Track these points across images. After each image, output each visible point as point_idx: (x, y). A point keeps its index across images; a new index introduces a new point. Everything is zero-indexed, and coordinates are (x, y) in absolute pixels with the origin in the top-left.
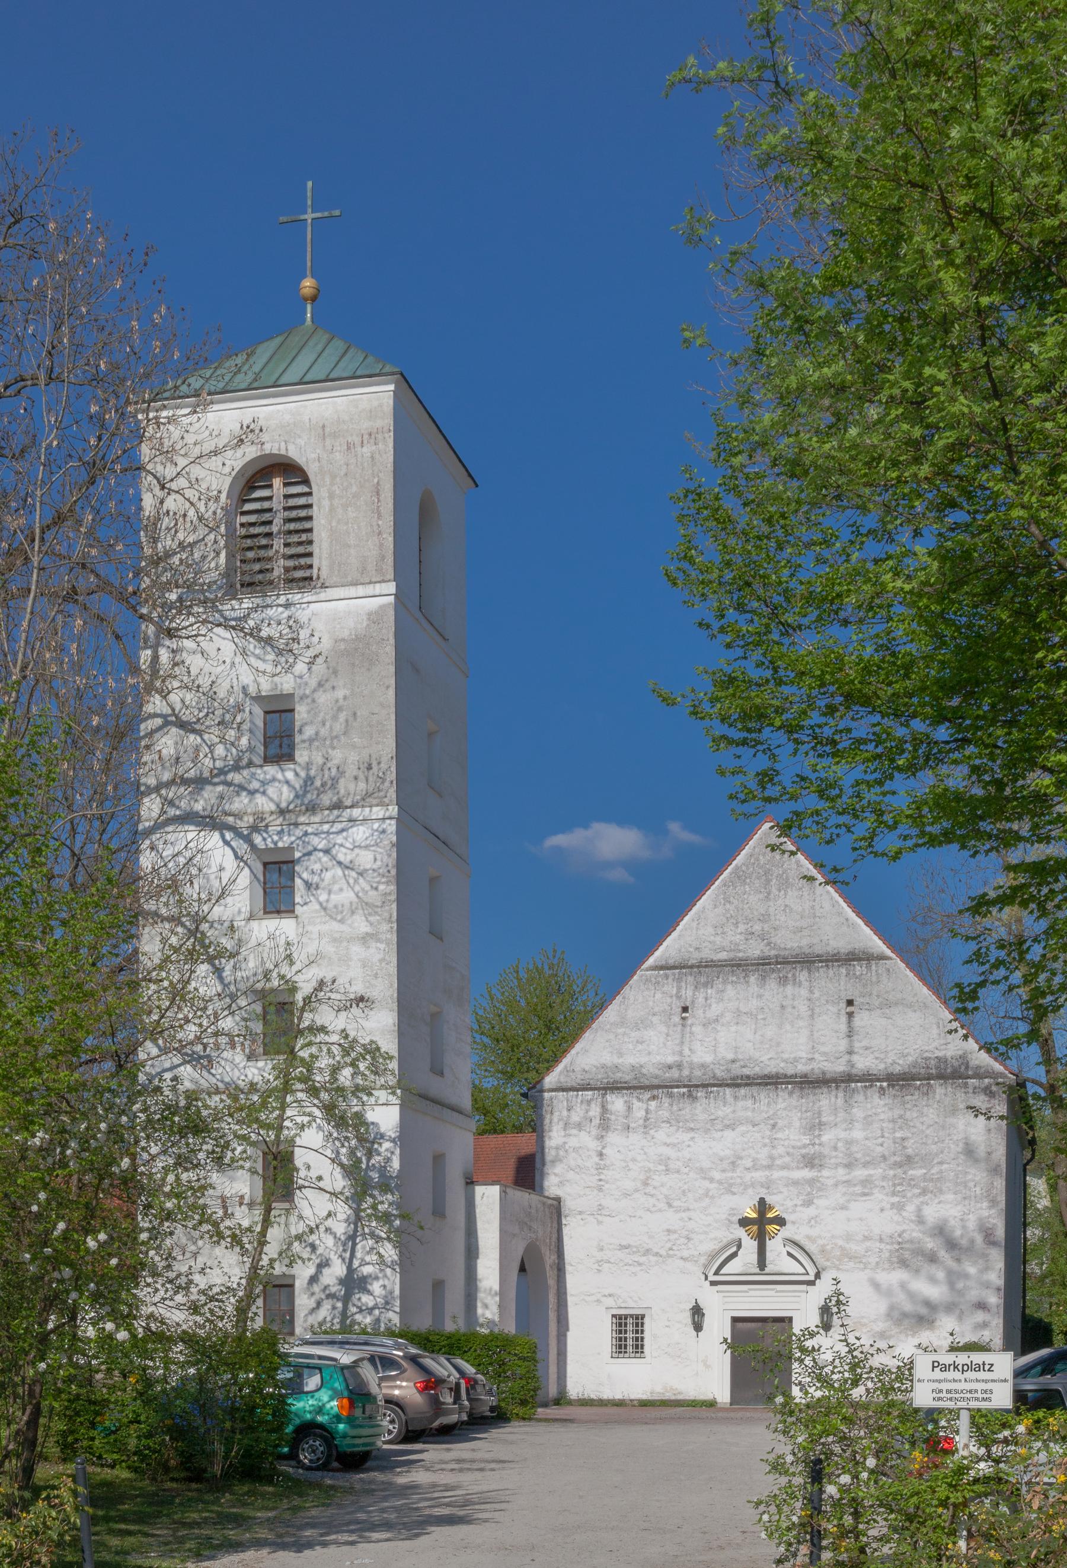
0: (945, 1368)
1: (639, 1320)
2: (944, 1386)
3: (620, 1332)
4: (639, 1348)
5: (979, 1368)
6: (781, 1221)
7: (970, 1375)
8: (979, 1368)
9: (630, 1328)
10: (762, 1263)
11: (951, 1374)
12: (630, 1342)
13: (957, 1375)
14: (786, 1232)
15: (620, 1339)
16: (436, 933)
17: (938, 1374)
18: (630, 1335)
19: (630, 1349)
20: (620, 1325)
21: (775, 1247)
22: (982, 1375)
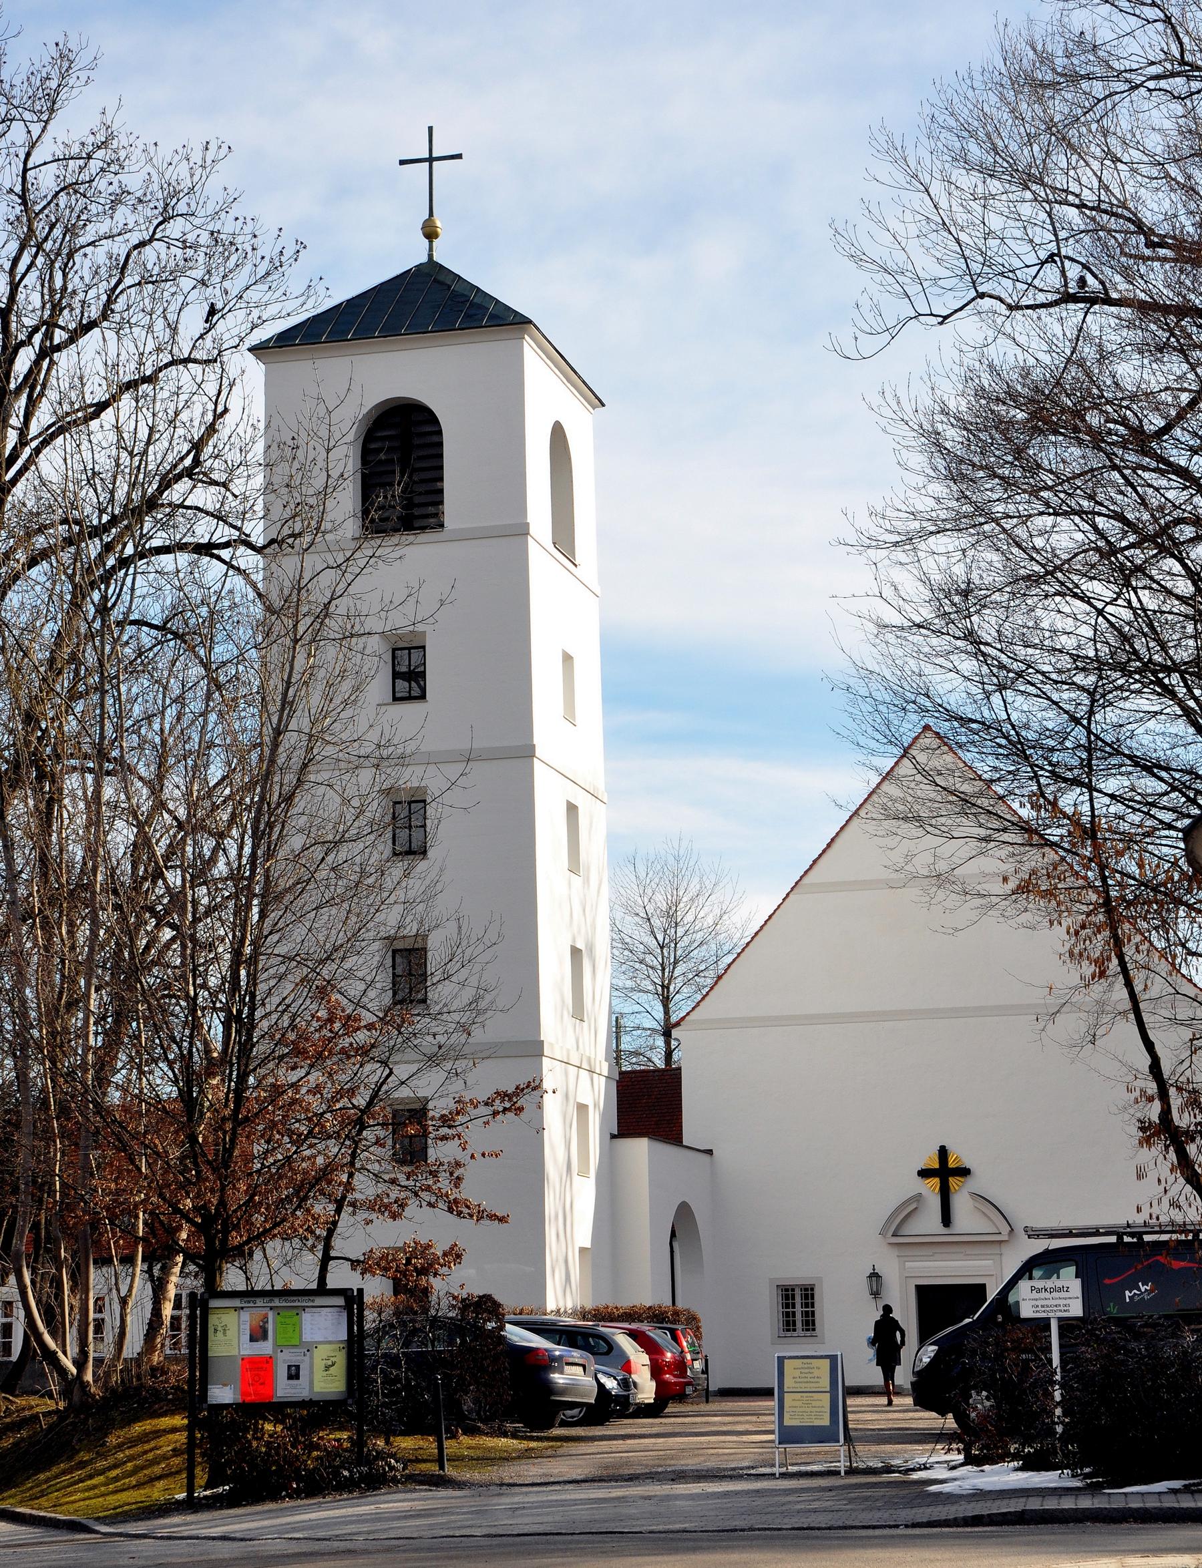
0: (1039, 1291)
1: (809, 1293)
2: (1039, 1303)
3: (787, 1306)
4: (786, 1293)
5: (1060, 1290)
6: (964, 1172)
7: (1055, 1295)
8: (1060, 1290)
9: (798, 1300)
10: (946, 1219)
11: (1043, 1295)
12: (799, 1317)
13: (1047, 1295)
14: (972, 1184)
15: (787, 1314)
16: (576, 953)
17: (1035, 1295)
18: (799, 1309)
19: (799, 1325)
20: (787, 1297)
21: (961, 1202)
22: (1063, 1294)
